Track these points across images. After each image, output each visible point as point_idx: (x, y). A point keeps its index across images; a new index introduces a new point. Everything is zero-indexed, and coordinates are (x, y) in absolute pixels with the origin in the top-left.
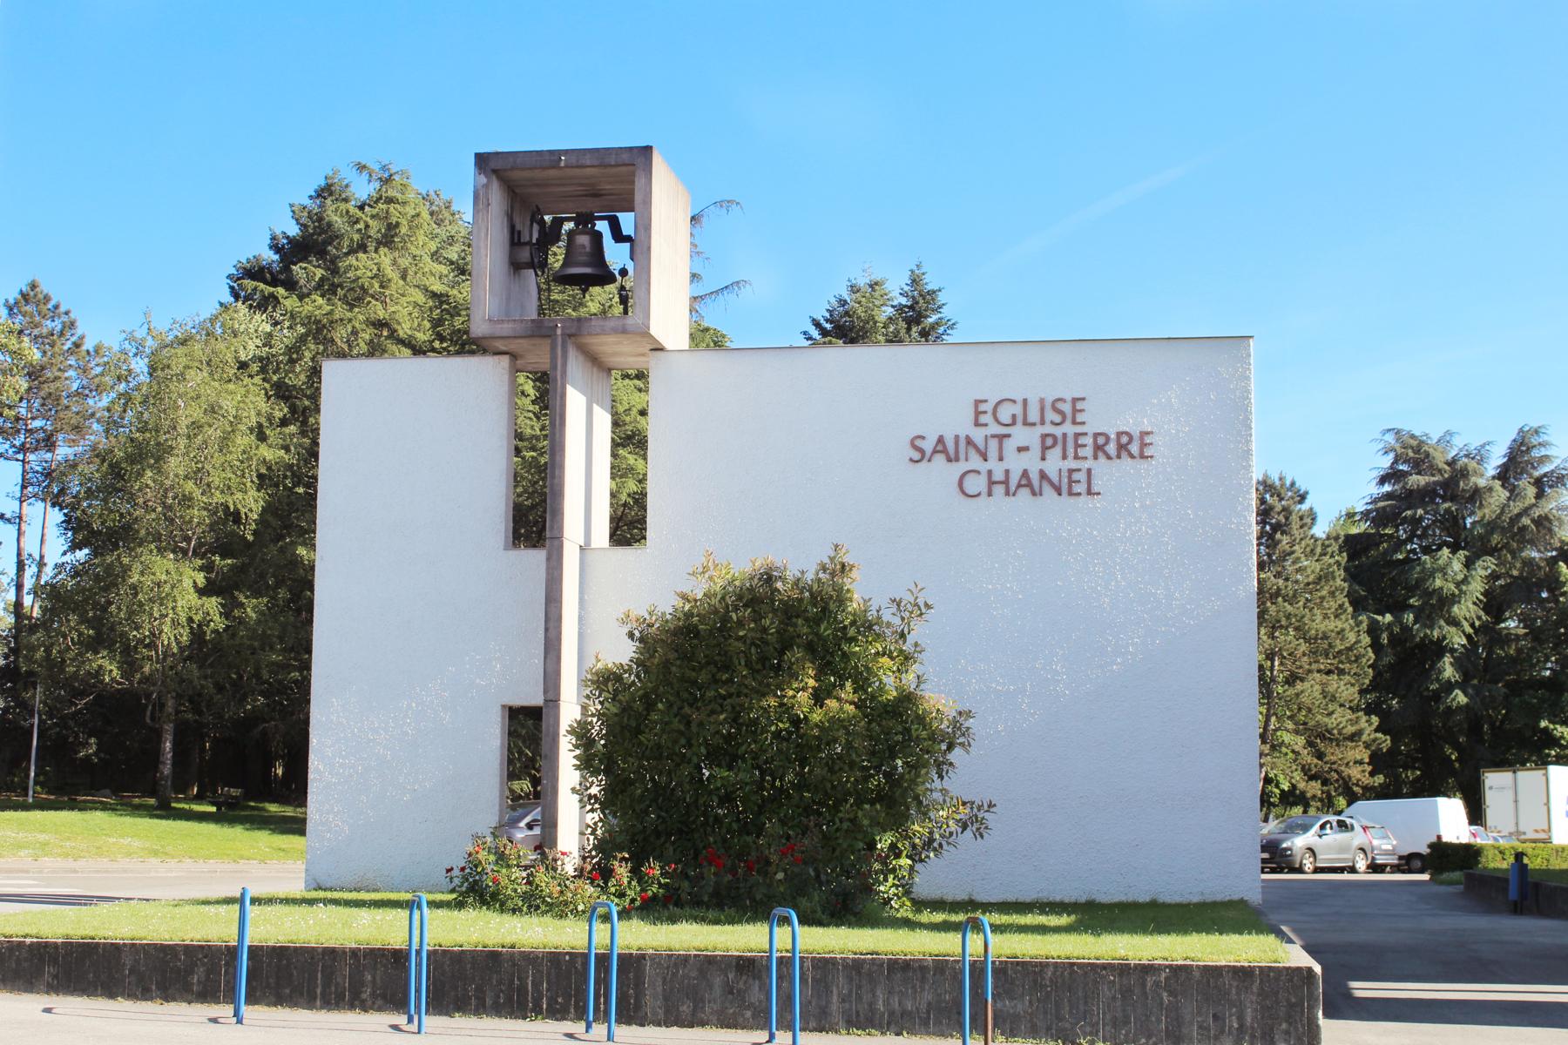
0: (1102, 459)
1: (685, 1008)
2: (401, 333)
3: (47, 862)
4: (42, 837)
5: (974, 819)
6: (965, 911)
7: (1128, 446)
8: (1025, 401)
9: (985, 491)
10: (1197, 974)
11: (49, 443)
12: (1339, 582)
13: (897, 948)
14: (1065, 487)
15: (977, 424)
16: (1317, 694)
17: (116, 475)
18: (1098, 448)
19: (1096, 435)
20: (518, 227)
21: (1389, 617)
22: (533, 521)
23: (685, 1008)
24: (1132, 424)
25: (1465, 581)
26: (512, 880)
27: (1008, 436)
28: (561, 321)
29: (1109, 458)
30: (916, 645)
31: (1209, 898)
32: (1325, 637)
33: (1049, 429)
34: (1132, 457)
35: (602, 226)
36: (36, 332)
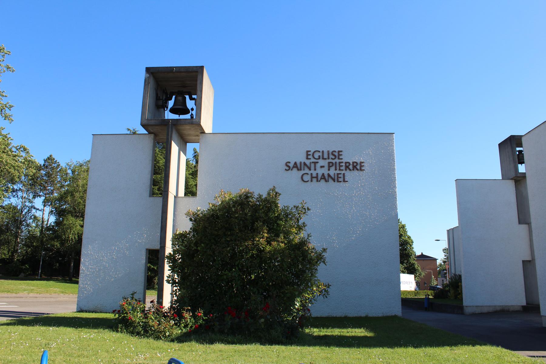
0: (348, 171)
4: (32, 288)
7: (357, 167)
8: (323, 151)
14: (336, 179)
15: (307, 158)
18: (347, 167)
19: (346, 163)
20: (159, 95)
22: (159, 184)
27: (318, 162)
30: (304, 223)
33: (330, 160)
34: (358, 170)
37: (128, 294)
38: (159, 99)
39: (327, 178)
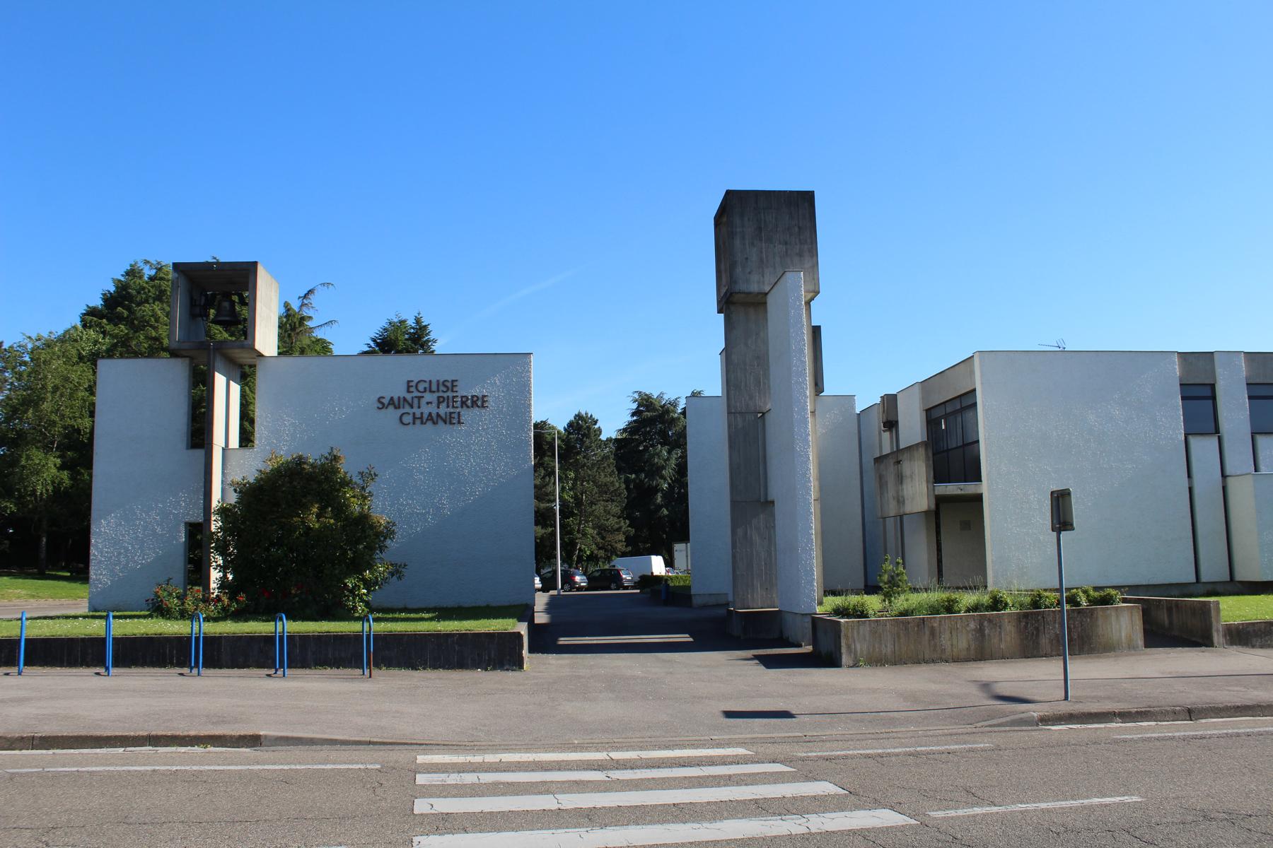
5: (397, 571)
7: (478, 402)
14: (449, 420)
18: (463, 403)
22: (200, 434)
24: (477, 391)
25: (668, 459)
33: (441, 394)
35: (235, 298)
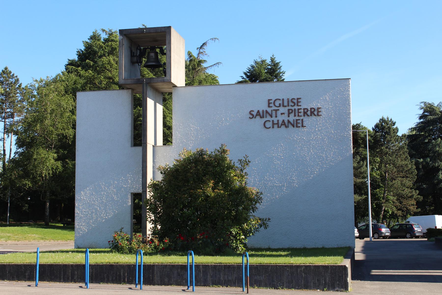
0: (306, 116)
1: (166, 280)
2: (115, 80)
3: (9, 242)
4: (8, 235)
6: (257, 250)
7: (314, 112)
8: (283, 99)
9: (271, 126)
10: (312, 268)
11: (12, 116)
12: (406, 150)
13: (215, 261)
14: (296, 124)
15: (269, 107)
16: (399, 184)
17: (29, 125)
18: (305, 113)
19: (304, 109)
21: (422, 160)
22: (139, 137)
23: (166, 280)
24: (314, 105)
26: (124, 243)
27: (278, 110)
28: (145, 79)
29: (308, 116)
31: (340, 246)
32: (402, 166)
33: (290, 108)
34: (315, 115)
35: (158, 50)
36: (7, 82)
37: (118, 229)
38: (134, 56)
39: (287, 124)
